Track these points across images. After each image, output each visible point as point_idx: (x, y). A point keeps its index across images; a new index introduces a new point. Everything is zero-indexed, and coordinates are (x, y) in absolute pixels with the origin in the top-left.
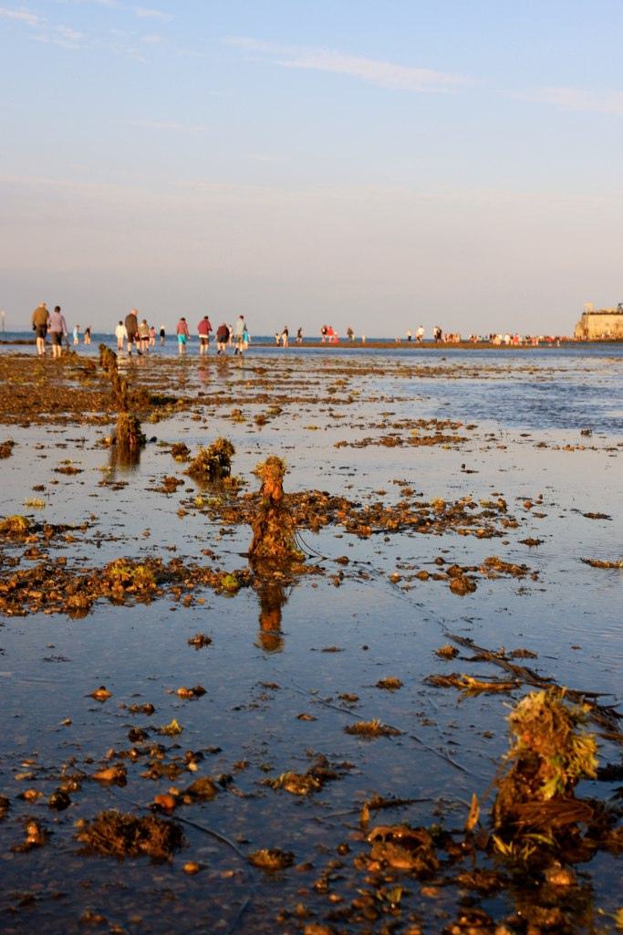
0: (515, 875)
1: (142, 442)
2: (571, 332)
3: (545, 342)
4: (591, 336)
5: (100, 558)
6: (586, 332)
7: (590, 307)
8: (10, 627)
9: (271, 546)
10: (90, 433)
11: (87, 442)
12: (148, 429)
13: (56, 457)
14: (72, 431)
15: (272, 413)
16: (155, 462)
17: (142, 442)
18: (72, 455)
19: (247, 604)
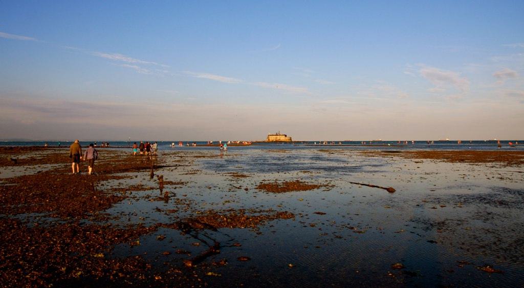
0: (231, 216)
1: (154, 175)
2: (266, 140)
3: (253, 143)
4: (271, 140)
5: (146, 187)
6: (269, 140)
7: (270, 134)
8: (197, 203)
9: (161, 186)
10: (147, 173)
11: (147, 174)
12: (155, 173)
13: (143, 177)
14: (145, 173)
15: (120, 199)
16: (155, 178)
17: (154, 175)
18: (145, 177)
19: (159, 190)
